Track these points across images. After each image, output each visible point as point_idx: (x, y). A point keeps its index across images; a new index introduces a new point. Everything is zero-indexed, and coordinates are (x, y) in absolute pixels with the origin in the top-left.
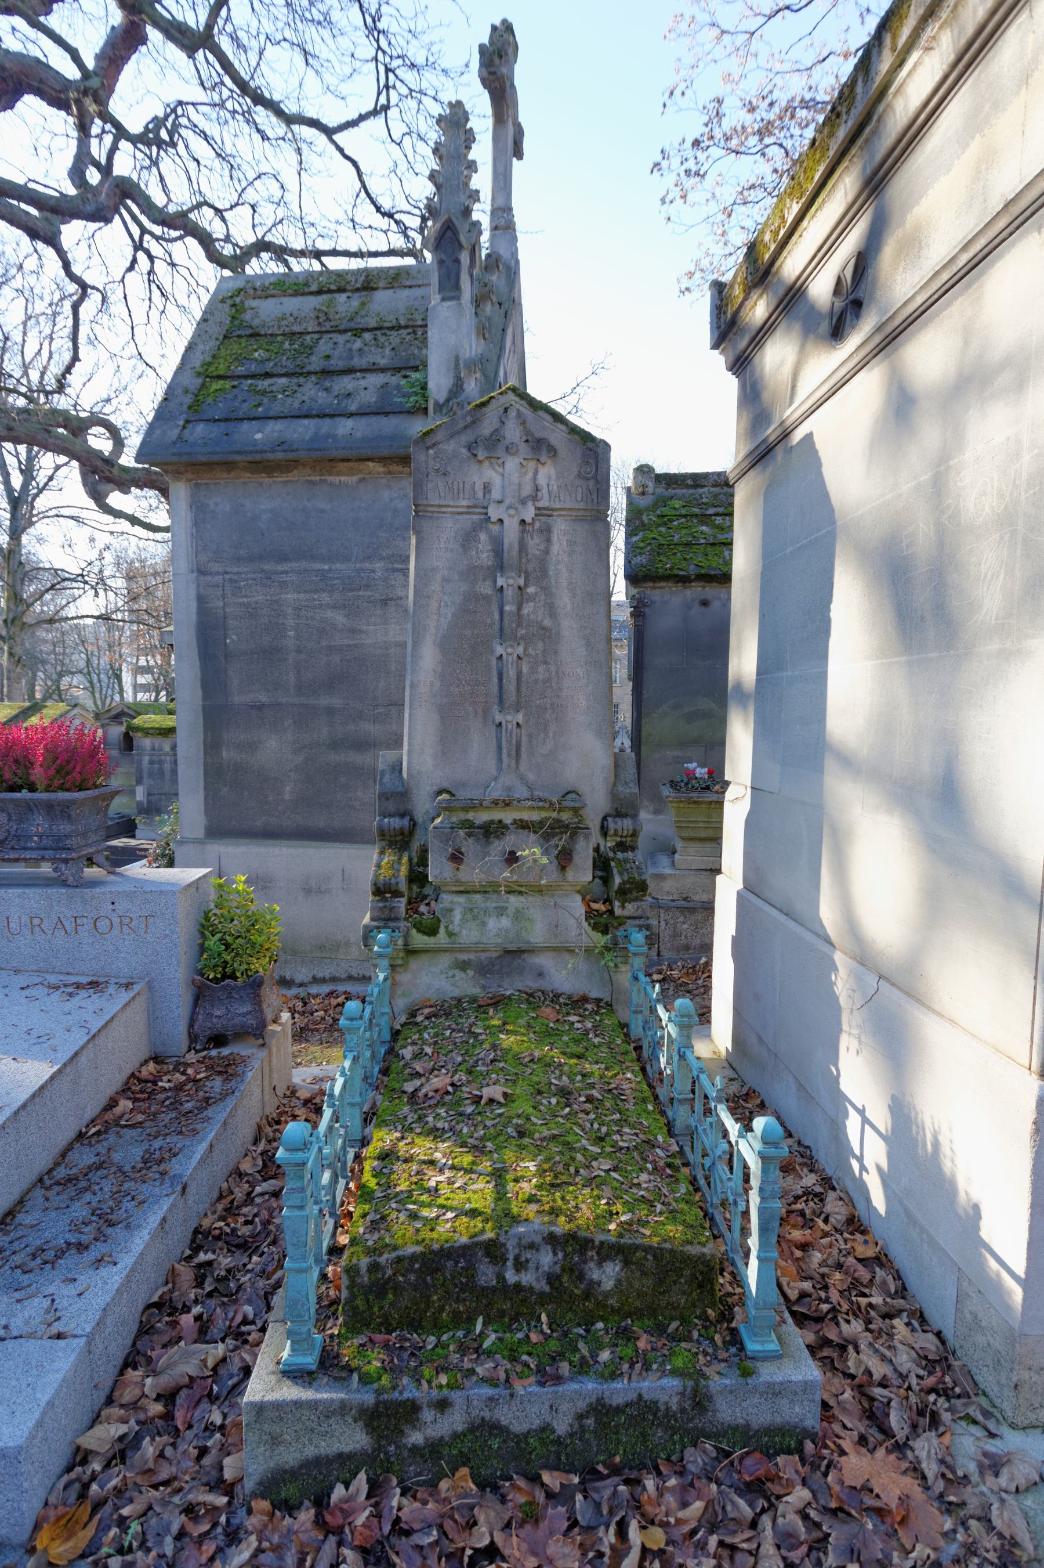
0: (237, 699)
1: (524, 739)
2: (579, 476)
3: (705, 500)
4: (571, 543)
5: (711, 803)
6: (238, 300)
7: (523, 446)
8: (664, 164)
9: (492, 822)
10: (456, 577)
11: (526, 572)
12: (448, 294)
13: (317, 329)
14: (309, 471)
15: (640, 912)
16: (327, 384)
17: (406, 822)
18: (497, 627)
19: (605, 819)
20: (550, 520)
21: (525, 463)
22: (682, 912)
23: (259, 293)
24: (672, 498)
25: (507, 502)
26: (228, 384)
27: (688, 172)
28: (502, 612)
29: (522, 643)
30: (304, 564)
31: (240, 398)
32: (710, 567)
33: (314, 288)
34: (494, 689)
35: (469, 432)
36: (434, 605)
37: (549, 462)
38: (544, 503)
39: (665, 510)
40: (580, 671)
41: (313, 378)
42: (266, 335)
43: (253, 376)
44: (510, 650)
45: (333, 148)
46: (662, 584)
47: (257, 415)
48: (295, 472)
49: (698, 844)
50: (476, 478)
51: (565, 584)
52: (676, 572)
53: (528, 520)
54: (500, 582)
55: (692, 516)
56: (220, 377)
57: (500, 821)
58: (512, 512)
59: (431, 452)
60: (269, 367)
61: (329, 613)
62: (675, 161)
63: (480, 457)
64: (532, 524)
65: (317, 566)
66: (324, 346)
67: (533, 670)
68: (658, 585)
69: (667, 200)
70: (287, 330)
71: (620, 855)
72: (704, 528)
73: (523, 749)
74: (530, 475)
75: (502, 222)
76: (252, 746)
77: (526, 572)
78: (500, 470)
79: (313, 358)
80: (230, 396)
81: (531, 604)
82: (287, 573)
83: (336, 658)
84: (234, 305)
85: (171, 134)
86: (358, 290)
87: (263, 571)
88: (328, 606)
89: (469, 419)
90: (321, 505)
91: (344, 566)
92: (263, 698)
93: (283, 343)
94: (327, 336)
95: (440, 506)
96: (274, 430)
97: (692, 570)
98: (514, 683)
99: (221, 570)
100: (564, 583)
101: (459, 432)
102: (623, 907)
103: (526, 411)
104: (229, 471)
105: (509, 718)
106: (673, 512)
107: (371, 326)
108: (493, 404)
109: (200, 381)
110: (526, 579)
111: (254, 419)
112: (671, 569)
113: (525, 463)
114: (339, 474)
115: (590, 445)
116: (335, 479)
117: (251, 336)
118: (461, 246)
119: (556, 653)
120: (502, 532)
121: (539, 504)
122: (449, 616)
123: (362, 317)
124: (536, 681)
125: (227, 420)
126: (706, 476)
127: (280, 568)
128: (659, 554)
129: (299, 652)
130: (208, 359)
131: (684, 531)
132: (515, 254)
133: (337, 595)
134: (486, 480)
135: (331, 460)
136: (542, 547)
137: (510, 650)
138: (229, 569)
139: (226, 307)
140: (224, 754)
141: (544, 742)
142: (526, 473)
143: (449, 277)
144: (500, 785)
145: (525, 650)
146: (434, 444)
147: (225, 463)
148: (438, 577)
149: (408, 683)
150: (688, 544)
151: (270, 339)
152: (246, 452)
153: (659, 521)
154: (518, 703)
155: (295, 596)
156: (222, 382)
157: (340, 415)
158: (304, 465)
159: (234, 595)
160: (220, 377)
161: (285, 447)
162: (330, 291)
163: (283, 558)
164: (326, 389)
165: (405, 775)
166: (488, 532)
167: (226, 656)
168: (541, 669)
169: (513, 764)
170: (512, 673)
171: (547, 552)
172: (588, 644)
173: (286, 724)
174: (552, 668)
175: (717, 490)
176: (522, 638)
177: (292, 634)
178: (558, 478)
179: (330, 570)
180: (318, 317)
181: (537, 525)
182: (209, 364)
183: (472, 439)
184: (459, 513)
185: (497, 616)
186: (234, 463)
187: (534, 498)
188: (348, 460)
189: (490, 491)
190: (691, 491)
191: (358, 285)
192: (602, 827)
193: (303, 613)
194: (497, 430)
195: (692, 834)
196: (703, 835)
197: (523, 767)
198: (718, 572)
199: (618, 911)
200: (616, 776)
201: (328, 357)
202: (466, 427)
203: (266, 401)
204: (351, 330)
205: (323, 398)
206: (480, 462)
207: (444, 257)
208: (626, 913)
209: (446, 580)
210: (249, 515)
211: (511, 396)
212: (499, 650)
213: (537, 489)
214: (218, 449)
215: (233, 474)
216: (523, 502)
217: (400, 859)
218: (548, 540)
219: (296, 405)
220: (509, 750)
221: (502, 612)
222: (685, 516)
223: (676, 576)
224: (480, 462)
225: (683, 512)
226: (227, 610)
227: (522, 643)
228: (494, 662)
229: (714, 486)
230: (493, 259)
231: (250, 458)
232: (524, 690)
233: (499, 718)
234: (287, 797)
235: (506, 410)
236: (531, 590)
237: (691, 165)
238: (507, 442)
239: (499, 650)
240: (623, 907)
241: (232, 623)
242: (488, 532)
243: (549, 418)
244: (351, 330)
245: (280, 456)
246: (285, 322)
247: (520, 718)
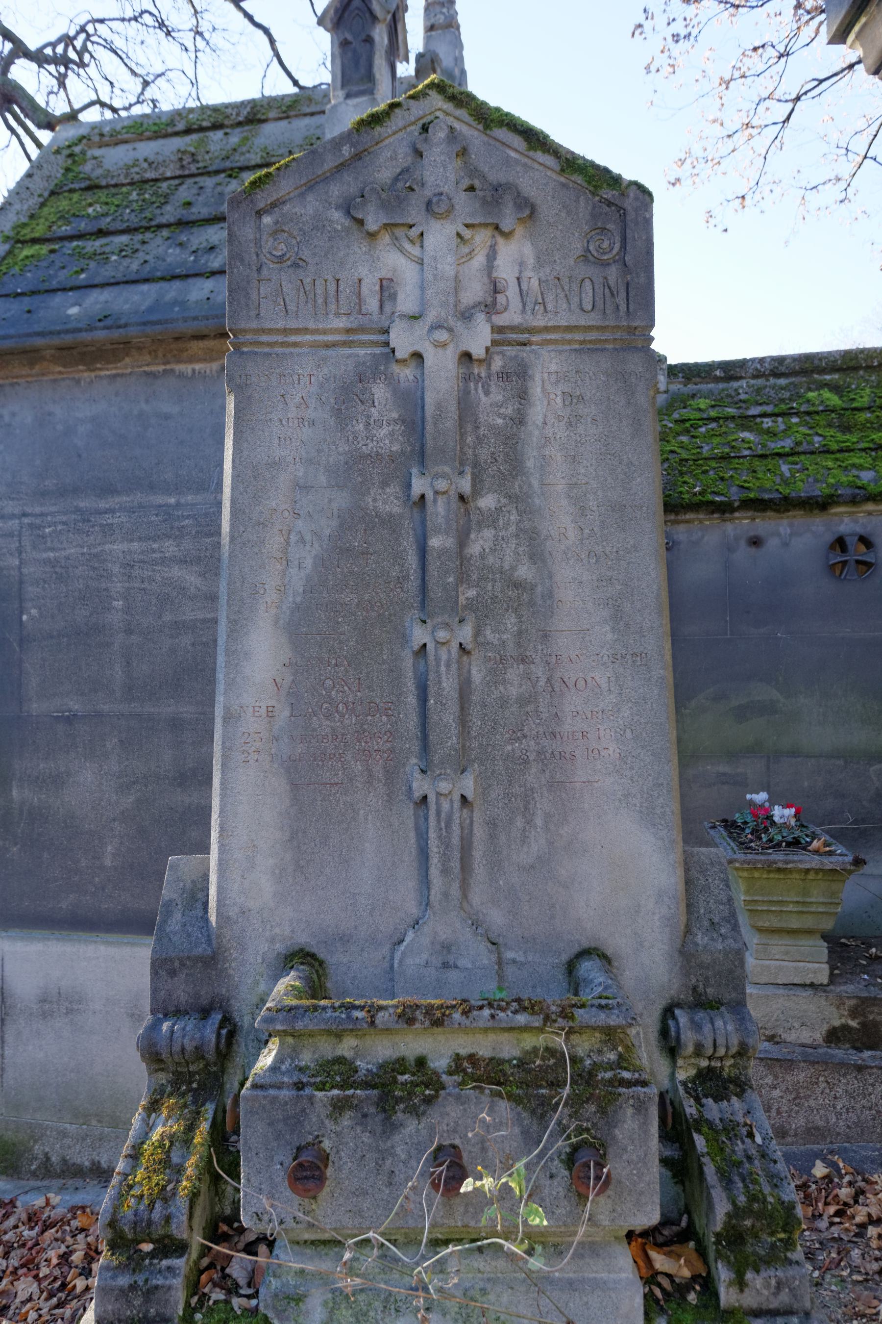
0: (35, 707)
1: (479, 833)
2: (585, 257)
3: (743, 397)
4: (570, 399)
5: (807, 871)
6: (77, 149)
7: (461, 199)
8: (648, 25)
9: (399, 1065)
10: (323, 479)
11: (475, 465)
12: (355, 89)
13: (178, 173)
14: (148, 358)
15: (784, 1298)
16: (183, 238)
17: (210, 1032)
18: (413, 584)
19: (668, 1012)
20: (524, 353)
21: (467, 233)
22: (770, 1068)
23: (107, 139)
24: (693, 396)
25: (432, 316)
26: (44, 249)
27: (676, 38)
28: (423, 551)
29: (471, 618)
30: (139, 497)
31: (58, 264)
32: (761, 489)
33: (181, 126)
34: (412, 722)
35: (347, 177)
36: (274, 542)
37: (520, 231)
38: (512, 316)
39: (685, 413)
40: (601, 677)
41: (165, 233)
42: (107, 186)
43: (80, 236)
44: (442, 635)
45: (240, 15)
46: (689, 516)
47: (78, 283)
48: (127, 360)
49: (787, 940)
50: (363, 271)
51: (561, 487)
52: (710, 497)
53: (478, 351)
54: (419, 486)
55: (726, 418)
56: (34, 241)
57: (421, 1062)
58: (442, 336)
59: (267, 220)
60: (104, 223)
61: (176, 572)
62: (660, 20)
63: (372, 225)
64: (486, 361)
65: (159, 499)
66: (185, 192)
67: (496, 676)
68: (682, 517)
69: (653, 68)
70: (137, 178)
71: (713, 1110)
72: (746, 435)
73: (478, 854)
74: (479, 259)
75: (441, 19)
76: (58, 781)
77: (475, 465)
78: (415, 251)
79: (168, 208)
80: (44, 264)
81: (488, 533)
82: (112, 511)
83: (186, 640)
84: (71, 155)
85: (80, 54)
86: (240, 124)
87: (78, 510)
88: (174, 560)
89: (347, 151)
90: (166, 408)
91: (199, 498)
92: (75, 705)
93: (129, 193)
94: (190, 181)
95: (285, 331)
96: (97, 300)
97: (734, 495)
98: (453, 707)
99: (17, 511)
100: (559, 483)
101: (326, 179)
102: (741, 1284)
103: (470, 132)
104: (32, 364)
105: (444, 786)
106: (698, 415)
107: (253, 163)
108: (399, 118)
109: (7, 247)
110: (476, 480)
111: (71, 289)
112: (702, 493)
113: (467, 233)
114: (191, 360)
115: (608, 194)
116: (186, 368)
117: (89, 188)
118: (374, 18)
119: (545, 636)
120: (420, 381)
121: (501, 320)
122: (309, 563)
123: (243, 154)
124: (504, 702)
125: (33, 293)
126: (742, 364)
127: (103, 505)
128: (682, 474)
129: (129, 632)
130: (24, 220)
131: (716, 440)
132: (459, 60)
133: (187, 544)
134: (384, 274)
135: (177, 339)
136: (509, 411)
137: (442, 635)
138: (29, 510)
139: (60, 159)
140: (15, 793)
141: (524, 839)
142: (471, 254)
143: (357, 63)
144: (426, 941)
145: (477, 633)
146: (274, 205)
147: (25, 352)
148: (284, 480)
149: (219, 712)
150: (725, 458)
151: (113, 190)
152: (51, 333)
153: (678, 428)
154: (464, 749)
155: (125, 546)
156: (37, 247)
157: (196, 275)
158: (139, 349)
159: (34, 548)
160: (34, 241)
161: (108, 322)
162: (202, 129)
163: (108, 490)
164: (181, 245)
165: (213, 918)
166: (391, 381)
167: (21, 641)
168: (514, 674)
169: (455, 890)
170: (449, 684)
171: (520, 420)
172: (617, 616)
173: (109, 746)
174: (539, 671)
175: (760, 382)
176: (470, 606)
177: (119, 604)
178: (540, 262)
179: (178, 505)
180: (181, 159)
181: (497, 363)
182: (24, 225)
183: (354, 190)
184: (328, 346)
185: (412, 560)
186: (36, 350)
187: (490, 308)
188: (202, 337)
189: (393, 297)
190: (721, 386)
191: (241, 119)
192: (664, 1033)
193: (136, 572)
194: (406, 170)
195: (775, 922)
196: (795, 924)
197: (476, 898)
198: (777, 496)
199: (727, 1296)
200: (690, 907)
201: (189, 204)
202: (341, 167)
203: (92, 264)
204: (224, 171)
205: (174, 256)
206: (372, 236)
207: (349, 37)
208: (749, 1300)
209: (301, 487)
210: (60, 427)
211: (436, 100)
212: (419, 635)
213: (496, 289)
214: (12, 331)
215: (37, 369)
216: (466, 316)
217: (191, 1128)
218: (523, 396)
219: (135, 266)
220: (445, 858)
221: (423, 551)
222: (715, 419)
223: (712, 503)
224: (372, 236)
225: (713, 413)
226: (25, 571)
227: (471, 618)
228: (408, 662)
229: (755, 377)
230: (428, 57)
231: (56, 341)
232: (476, 722)
233: (421, 786)
234: (108, 862)
235: (425, 129)
236: (487, 502)
237: (679, 28)
238: (428, 193)
239: (419, 635)
240: (741, 1284)
241: (31, 590)
242: (391, 381)
243: (517, 142)
244: (224, 171)
245: (101, 335)
246: (137, 169)
247: (468, 785)
